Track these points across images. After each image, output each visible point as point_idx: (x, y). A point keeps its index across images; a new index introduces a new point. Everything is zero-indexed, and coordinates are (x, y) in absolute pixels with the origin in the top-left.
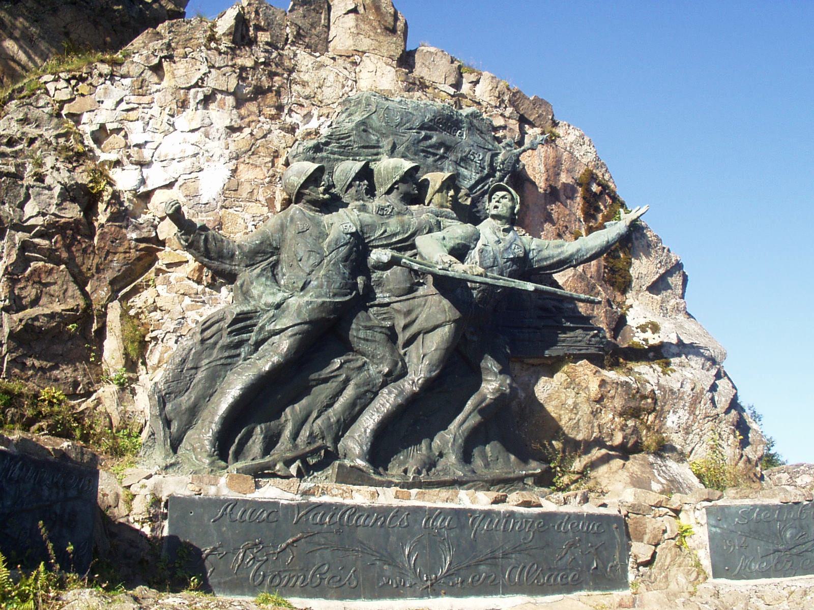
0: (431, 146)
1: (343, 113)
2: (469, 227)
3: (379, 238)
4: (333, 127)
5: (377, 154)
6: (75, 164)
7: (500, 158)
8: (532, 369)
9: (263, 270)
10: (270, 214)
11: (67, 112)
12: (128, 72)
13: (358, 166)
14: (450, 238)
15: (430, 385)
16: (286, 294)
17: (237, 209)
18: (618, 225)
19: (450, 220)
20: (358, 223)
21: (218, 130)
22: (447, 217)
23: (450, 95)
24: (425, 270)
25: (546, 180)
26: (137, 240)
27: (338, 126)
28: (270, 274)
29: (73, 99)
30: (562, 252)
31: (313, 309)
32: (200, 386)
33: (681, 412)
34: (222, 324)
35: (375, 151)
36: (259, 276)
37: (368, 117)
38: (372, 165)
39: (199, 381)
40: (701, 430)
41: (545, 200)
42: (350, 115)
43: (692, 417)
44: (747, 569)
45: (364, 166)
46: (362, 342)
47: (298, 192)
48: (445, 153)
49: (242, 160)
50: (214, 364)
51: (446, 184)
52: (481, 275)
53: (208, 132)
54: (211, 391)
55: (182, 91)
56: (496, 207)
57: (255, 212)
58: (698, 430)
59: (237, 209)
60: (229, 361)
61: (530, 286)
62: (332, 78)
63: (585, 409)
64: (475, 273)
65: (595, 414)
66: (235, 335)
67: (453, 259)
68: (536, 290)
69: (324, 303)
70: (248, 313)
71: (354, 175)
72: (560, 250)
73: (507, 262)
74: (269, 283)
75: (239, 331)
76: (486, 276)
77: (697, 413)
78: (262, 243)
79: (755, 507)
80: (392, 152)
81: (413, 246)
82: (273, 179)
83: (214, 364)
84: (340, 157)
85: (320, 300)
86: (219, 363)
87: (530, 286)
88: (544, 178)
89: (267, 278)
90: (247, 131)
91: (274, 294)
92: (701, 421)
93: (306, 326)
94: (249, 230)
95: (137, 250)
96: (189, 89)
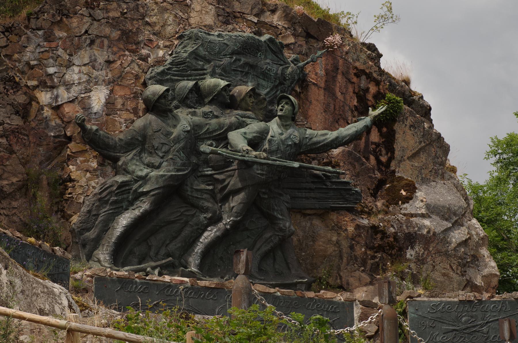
0: (240, 66)
1: (179, 45)
2: (262, 124)
3: (205, 133)
4: (174, 56)
5: (204, 74)
6: (15, 90)
7: (290, 69)
8: (308, 217)
9: (135, 155)
10: (135, 118)
11: (4, 54)
12: (42, 26)
13: (191, 84)
14: (250, 133)
15: (235, 226)
16: (148, 170)
17: (115, 116)
18: (366, 120)
19: (250, 120)
20: (192, 124)
21: (100, 63)
22: (249, 117)
23: (255, 23)
24: (229, 156)
25: (326, 81)
26: (54, 137)
27: (176, 55)
28: (138, 158)
29: (8, 45)
30: (326, 139)
31: (166, 179)
32: (100, 225)
33: (417, 248)
34: (111, 188)
35: (201, 72)
36: (132, 158)
37: (196, 49)
38: (200, 83)
39: (99, 223)
40: (434, 262)
41: (325, 96)
42: (185, 47)
43: (426, 252)
44: (434, 340)
45: (195, 84)
46: (195, 199)
47: (154, 105)
48: (248, 70)
49: (116, 83)
50: (107, 212)
51: (249, 94)
52: (264, 159)
53: (95, 65)
54: (106, 229)
55: (77, 38)
56: (281, 110)
57: (125, 117)
58: (432, 262)
59: (115, 116)
60: (116, 210)
61: (296, 165)
62: (171, 19)
63: (345, 244)
64: (263, 157)
65: (352, 247)
66: (120, 195)
67: (249, 148)
68: (301, 167)
69: (172, 175)
70: (127, 182)
71: (188, 91)
72: (324, 138)
73: (287, 147)
74: (138, 163)
75: (122, 193)
76: (268, 159)
77: (431, 249)
78: (132, 139)
79: (441, 302)
80: (213, 75)
81: (226, 138)
82: (136, 96)
83: (107, 212)
84: (179, 78)
85: (170, 174)
86: (110, 212)
87: (296, 165)
88: (324, 80)
89: (137, 160)
90: (119, 63)
91: (141, 170)
92: (434, 255)
93: (242, 205)
94: (123, 129)
95: (54, 143)
96: (80, 36)
